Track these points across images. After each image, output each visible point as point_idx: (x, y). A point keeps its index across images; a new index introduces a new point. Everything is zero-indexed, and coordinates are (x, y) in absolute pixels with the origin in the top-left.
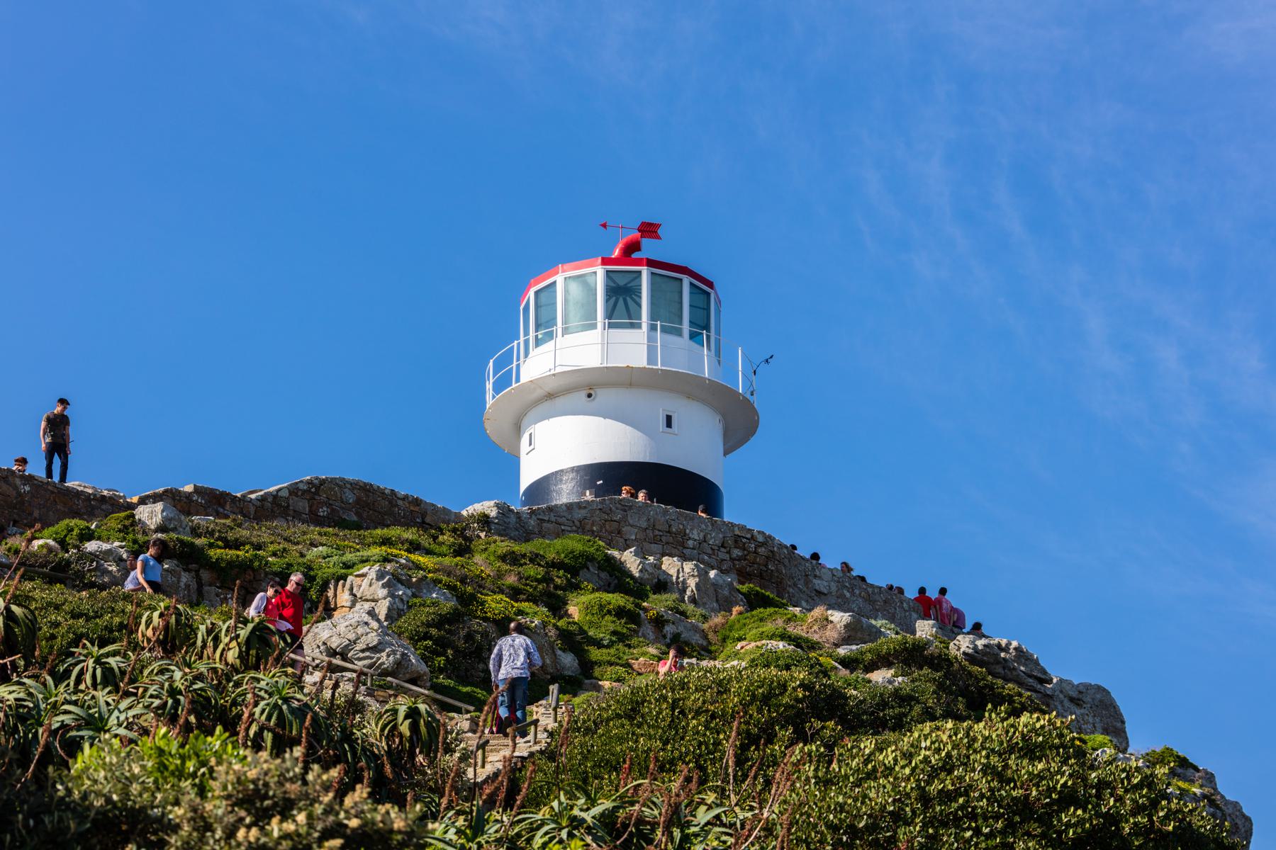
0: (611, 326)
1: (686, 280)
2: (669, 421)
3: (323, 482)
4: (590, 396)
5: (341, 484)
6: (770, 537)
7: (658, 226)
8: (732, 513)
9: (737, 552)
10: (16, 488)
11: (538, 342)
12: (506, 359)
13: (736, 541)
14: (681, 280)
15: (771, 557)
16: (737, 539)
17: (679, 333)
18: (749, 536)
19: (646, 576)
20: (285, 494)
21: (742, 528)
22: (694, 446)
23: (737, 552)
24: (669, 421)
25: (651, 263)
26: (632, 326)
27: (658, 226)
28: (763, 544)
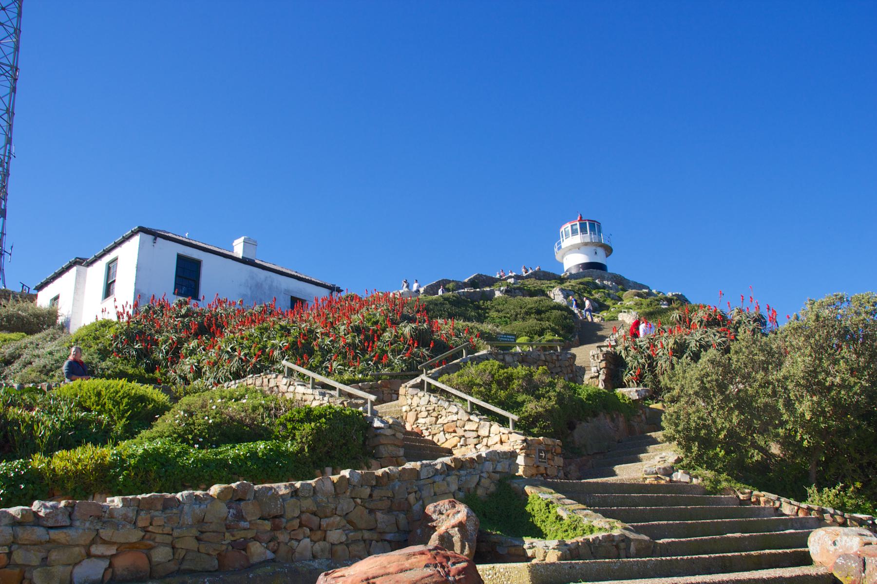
8: (610, 270)
22: (600, 258)
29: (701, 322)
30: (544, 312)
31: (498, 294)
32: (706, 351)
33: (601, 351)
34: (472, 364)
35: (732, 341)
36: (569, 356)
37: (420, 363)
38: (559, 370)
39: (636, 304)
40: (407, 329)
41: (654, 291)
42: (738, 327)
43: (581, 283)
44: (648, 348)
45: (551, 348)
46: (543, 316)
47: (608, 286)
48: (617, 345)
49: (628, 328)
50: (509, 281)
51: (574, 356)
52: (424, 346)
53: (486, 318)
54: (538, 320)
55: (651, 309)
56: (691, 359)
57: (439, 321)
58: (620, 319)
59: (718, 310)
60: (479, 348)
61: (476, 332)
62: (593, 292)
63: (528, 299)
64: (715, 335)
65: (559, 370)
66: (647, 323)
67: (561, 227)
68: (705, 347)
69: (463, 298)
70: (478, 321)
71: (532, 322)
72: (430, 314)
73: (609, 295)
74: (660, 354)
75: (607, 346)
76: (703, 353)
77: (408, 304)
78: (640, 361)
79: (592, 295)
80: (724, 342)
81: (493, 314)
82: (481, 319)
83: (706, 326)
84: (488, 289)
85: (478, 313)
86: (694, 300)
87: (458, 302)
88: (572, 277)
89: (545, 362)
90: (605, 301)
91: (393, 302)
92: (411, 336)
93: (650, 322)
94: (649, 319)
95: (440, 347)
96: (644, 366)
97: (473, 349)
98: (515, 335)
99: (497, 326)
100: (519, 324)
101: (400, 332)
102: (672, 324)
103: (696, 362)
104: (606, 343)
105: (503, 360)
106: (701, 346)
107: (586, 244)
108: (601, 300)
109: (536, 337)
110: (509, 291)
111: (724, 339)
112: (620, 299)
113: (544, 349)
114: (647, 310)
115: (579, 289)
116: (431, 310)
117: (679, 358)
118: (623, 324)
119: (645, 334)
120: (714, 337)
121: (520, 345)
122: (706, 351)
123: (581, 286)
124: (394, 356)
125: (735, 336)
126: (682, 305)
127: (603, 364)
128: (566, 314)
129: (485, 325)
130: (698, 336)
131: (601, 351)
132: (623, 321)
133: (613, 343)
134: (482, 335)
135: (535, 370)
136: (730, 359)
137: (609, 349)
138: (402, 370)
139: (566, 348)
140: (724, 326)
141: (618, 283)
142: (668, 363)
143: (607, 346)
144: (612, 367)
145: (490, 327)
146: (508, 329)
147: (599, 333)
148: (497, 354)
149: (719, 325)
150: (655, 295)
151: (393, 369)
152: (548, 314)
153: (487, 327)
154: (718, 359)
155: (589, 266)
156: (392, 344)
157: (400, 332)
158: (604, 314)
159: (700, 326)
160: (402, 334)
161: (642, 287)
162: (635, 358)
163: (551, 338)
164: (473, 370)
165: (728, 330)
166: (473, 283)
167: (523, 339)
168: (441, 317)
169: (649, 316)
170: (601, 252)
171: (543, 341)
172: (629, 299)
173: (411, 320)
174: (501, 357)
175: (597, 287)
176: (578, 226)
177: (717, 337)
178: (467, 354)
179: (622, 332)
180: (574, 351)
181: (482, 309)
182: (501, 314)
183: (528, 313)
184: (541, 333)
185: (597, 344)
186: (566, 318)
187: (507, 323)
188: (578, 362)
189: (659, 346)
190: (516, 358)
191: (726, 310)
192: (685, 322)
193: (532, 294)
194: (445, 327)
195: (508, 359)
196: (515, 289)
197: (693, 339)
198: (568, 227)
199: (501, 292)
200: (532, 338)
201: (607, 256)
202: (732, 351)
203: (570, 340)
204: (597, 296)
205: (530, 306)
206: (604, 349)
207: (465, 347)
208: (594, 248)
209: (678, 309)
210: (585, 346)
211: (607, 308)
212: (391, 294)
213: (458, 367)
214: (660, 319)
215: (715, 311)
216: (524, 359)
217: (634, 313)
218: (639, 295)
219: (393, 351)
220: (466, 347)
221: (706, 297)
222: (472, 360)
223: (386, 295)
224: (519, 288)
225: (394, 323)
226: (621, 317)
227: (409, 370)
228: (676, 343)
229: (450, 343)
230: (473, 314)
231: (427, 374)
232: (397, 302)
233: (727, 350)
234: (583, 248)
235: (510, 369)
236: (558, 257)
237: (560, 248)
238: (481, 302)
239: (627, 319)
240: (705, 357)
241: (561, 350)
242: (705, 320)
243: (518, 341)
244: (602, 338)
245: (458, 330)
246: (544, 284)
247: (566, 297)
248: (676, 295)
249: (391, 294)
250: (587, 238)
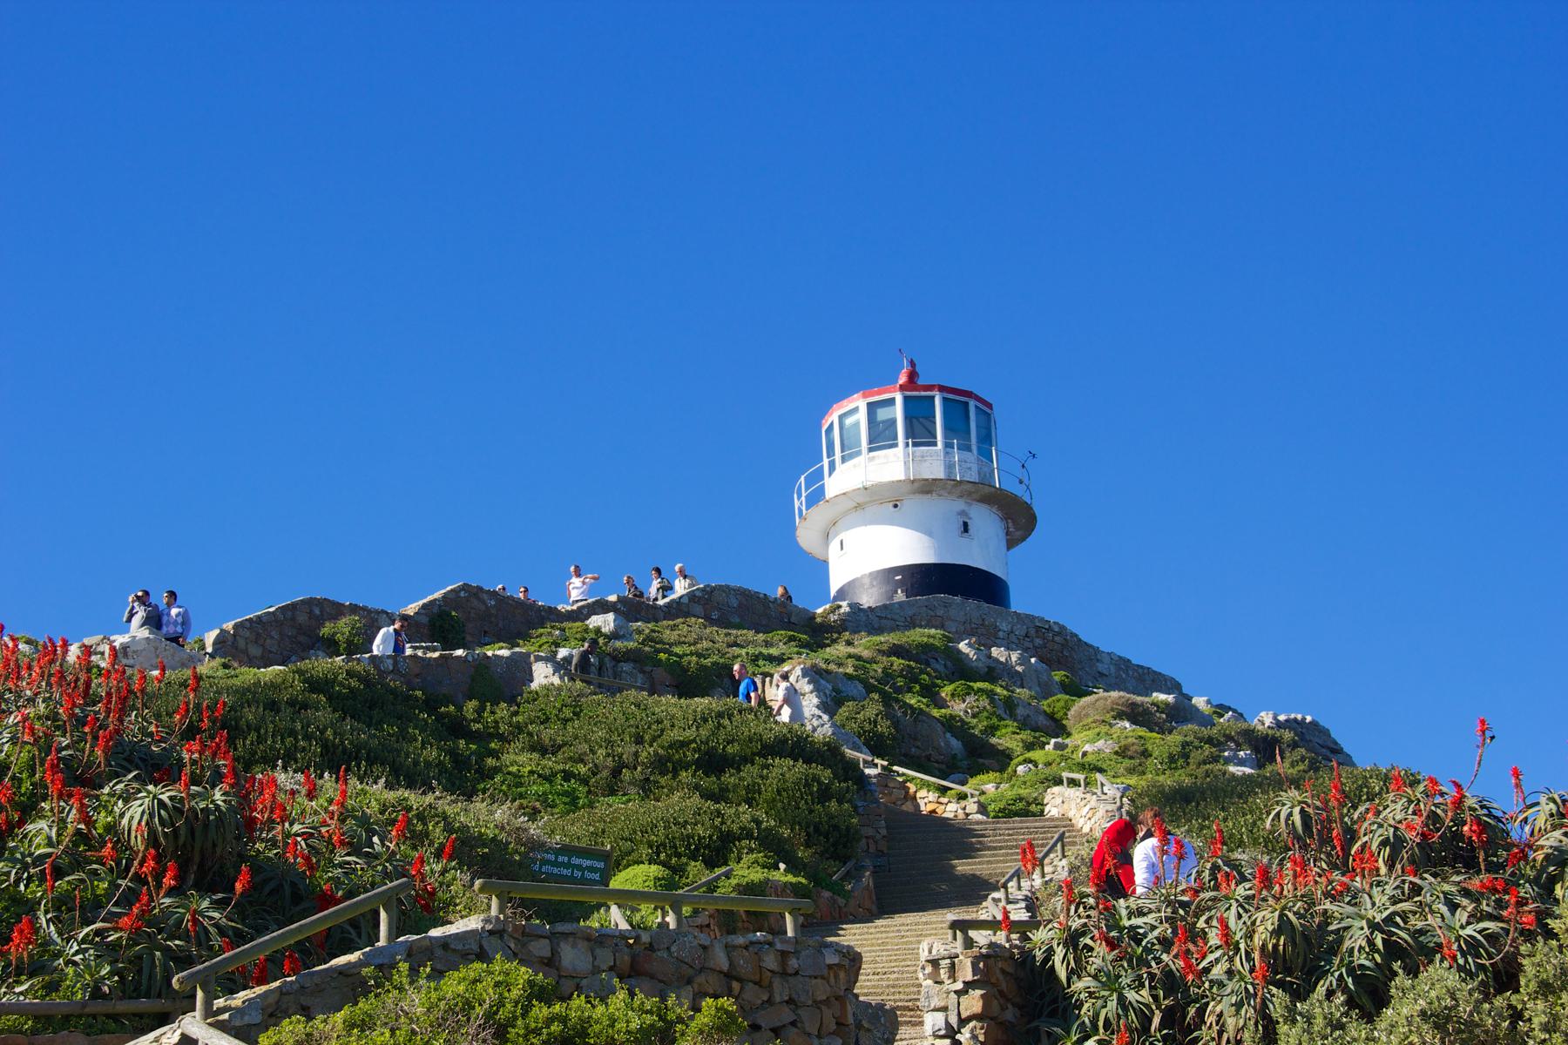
0: (915, 445)
1: (972, 403)
2: (965, 525)
3: (714, 589)
5: (726, 589)
8: (1019, 602)
9: (1038, 641)
10: (484, 602)
11: (844, 460)
12: (819, 476)
14: (967, 404)
15: (1065, 645)
16: (1038, 629)
17: (969, 449)
20: (685, 600)
21: (1042, 620)
22: (982, 550)
23: (1038, 641)
24: (965, 525)
25: (942, 389)
26: (891, 446)
28: (1059, 634)
29: (1395, 845)
30: (738, 763)
31: (542, 675)
32: (1413, 972)
33: (969, 943)
34: (414, 972)
35: (1529, 936)
36: (832, 959)
37: (184, 961)
38: (787, 1015)
39: (1122, 753)
40: (134, 811)
41: (1200, 702)
42: (1553, 880)
43: (896, 651)
44: (1166, 943)
45: (758, 920)
46: (729, 779)
47: (1007, 667)
48: (1034, 924)
49: (1086, 851)
50: (595, 621)
51: (853, 961)
52: (205, 888)
53: (490, 774)
54: (708, 795)
55: (1180, 778)
56: (1351, 1003)
57: (281, 777)
58: (1052, 811)
59: (1470, 802)
60: (451, 903)
61: (438, 833)
62: (946, 691)
63: (668, 703)
64: (1453, 907)
65: (787, 1015)
66: (1165, 836)
67: (825, 410)
68: (1412, 954)
69: (394, 683)
70: (450, 788)
71: (680, 802)
72: (244, 745)
73: (1010, 706)
74: (1218, 972)
75: (993, 925)
76: (1402, 980)
77: (148, 698)
78: (1131, 996)
79: (941, 704)
80: (1492, 938)
81: (518, 759)
82: (465, 778)
83: (1417, 866)
84: (505, 653)
85: (453, 753)
86: (1367, 751)
87: (370, 699)
88: (861, 620)
89: (729, 980)
90: (992, 730)
91: (78, 683)
92: (152, 840)
93: (1180, 832)
94: (1175, 820)
95: (280, 894)
96: (1146, 1020)
97: (423, 908)
98: (605, 857)
99: (534, 815)
100: (624, 809)
101: (102, 819)
102: (1271, 844)
103: (1369, 1017)
104: (989, 910)
105: (550, 963)
106: (1393, 950)
107: (926, 487)
108: (978, 726)
109: (695, 867)
110: (599, 667)
111: (1492, 926)
112: (1057, 727)
113: (728, 922)
114: (1168, 780)
115: (888, 675)
116: (241, 732)
117: (1300, 993)
118: (1064, 835)
119: (1157, 881)
120: (1450, 914)
121: (627, 899)
122: (1413, 972)
123: (898, 663)
124: (67, 934)
125: (1542, 916)
126: (1314, 767)
127: (973, 1003)
128: (826, 775)
129: (479, 805)
130: (1378, 903)
131: (969, 943)
132: (1066, 821)
133: (1019, 914)
134: (470, 852)
135: (683, 1010)
136: (1517, 1015)
137: (1001, 937)
138: (96, 993)
139: (821, 923)
140: (1493, 868)
141: (1050, 662)
142: (1248, 1011)
143: (993, 925)
144: (1010, 1014)
145: (501, 814)
146: (577, 829)
147: (963, 867)
148: (526, 935)
149: (1471, 865)
150: (1206, 721)
151: (52, 987)
152: (750, 772)
153: (489, 816)
154: (1465, 1009)
155: (926, 580)
156: (58, 873)
157: (102, 819)
158: (988, 785)
159: (1391, 866)
160: (111, 828)
161: (1149, 679)
162: (1110, 981)
163: (757, 875)
164: (416, 1001)
165: (1511, 885)
166: (440, 623)
167: (637, 876)
168: (289, 759)
169: (1174, 806)
170: (987, 523)
171: (726, 888)
172: (1093, 728)
173: (159, 769)
174: (541, 948)
175: (961, 671)
176: (898, 411)
177: (1461, 916)
178: (397, 930)
179: (1058, 867)
180: (852, 936)
181: (472, 737)
182: (550, 763)
183: (667, 765)
184: (717, 852)
185: (951, 915)
186: (825, 794)
187: (573, 804)
188: (868, 987)
189: (1214, 939)
190: (606, 957)
191: (1505, 802)
192: (1325, 840)
193: (687, 683)
194: (306, 805)
195: (572, 957)
196: (618, 657)
197: (1361, 917)
198: (854, 411)
199: (561, 667)
200: (679, 870)
201: (1011, 543)
202: (1528, 982)
203: (837, 889)
204: (958, 708)
205: (675, 735)
206: (981, 937)
207: (390, 900)
208: (960, 505)
209: (1296, 783)
210: (900, 919)
211: (1000, 761)
212: (74, 651)
213: (351, 986)
214: (1218, 821)
215: (1459, 802)
216: (638, 962)
217: (1111, 791)
218: (1136, 715)
219: (61, 904)
220: (390, 900)
221: (1420, 735)
222: (416, 956)
223: (51, 652)
224: (628, 656)
225: (80, 779)
226: (1061, 802)
227: (128, 989)
228: (1283, 927)
229: (324, 878)
230: (431, 754)
231: (209, 1012)
232: (99, 686)
233: (1505, 977)
234: (912, 504)
235: (578, 1002)
236: (807, 536)
237: (816, 497)
238: (471, 706)
239: (1085, 811)
240: (1409, 1001)
241: (801, 928)
242: (1412, 837)
243: (618, 882)
244: (975, 890)
245: (364, 821)
246: (738, 647)
247: (831, 705)
248: (1288, 725)
249: (74, 651)
250: (933, 462)
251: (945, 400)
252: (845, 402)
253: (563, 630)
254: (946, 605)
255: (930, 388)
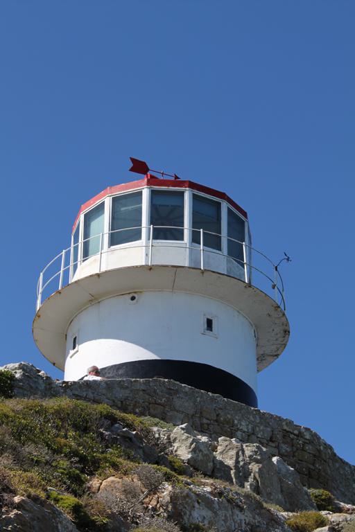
0: (156, 237)
2: (209, 324)
4: (133, 298)
6: (315, 435)
7: (132, 170)
8: (264, 405)
13: (284, 437)
14: (219, 204)
16: (286, 434)
17: (218, 247)
18: (296, 432)
19: (200, 457)
21: (290, 423)
22: (227, 353)
24: (209, 324)
25: (192, 185)
27: (132, 170)
28: (310, 442)
251: (195, 197)
252: (91, 201)
253: (254, 518)
254: (172, 392)
255: (181, 184)
